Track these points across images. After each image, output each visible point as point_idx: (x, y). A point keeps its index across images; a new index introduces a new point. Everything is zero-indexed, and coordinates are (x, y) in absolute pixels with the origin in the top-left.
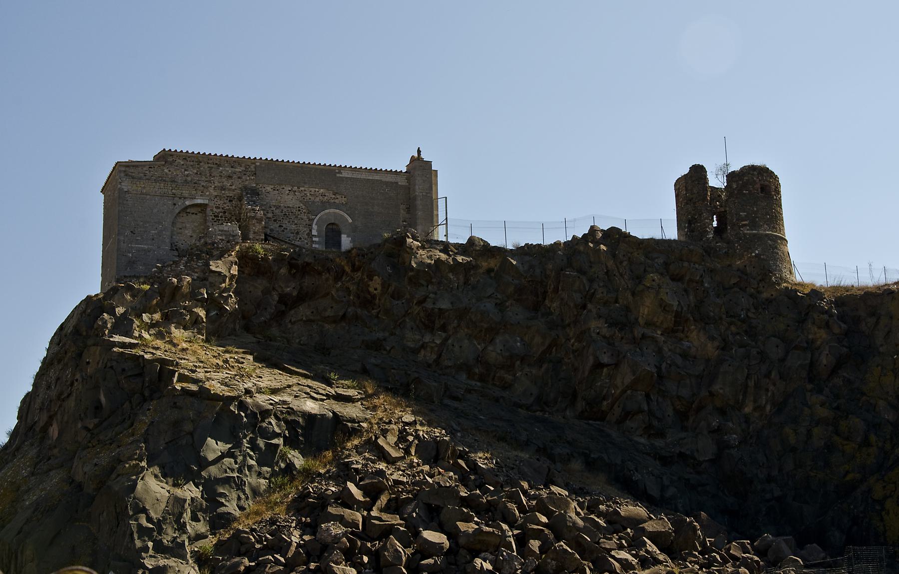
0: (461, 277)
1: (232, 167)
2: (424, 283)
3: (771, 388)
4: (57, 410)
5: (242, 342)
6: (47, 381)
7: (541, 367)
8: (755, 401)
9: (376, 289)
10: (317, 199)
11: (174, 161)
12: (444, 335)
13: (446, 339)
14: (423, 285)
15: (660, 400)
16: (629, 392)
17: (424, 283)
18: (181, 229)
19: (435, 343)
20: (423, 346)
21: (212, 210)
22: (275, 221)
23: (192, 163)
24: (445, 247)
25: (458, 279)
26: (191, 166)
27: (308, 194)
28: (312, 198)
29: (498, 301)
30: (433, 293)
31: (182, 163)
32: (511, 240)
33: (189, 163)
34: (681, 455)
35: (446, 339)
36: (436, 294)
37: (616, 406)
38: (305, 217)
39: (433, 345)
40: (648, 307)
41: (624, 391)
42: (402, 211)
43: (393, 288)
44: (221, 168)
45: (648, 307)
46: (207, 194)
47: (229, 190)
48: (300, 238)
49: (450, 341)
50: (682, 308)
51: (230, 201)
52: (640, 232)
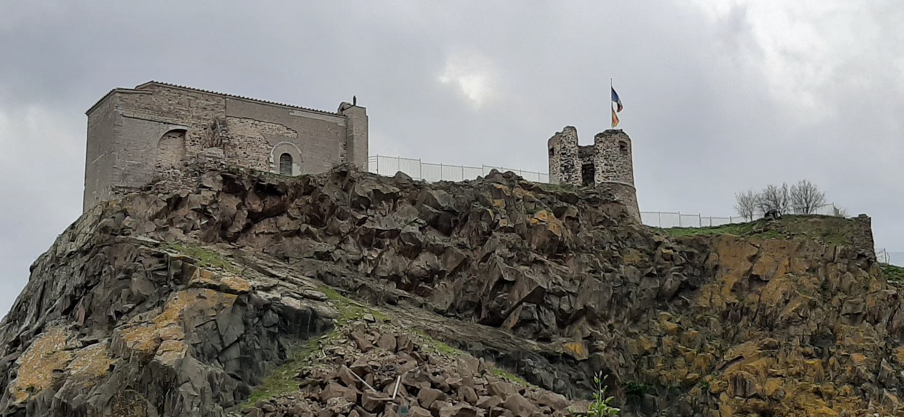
0: (392, 205)
1: (207, 100)
2: (364, 208)
3: (630, 305)
4: (539, 317)
5: (146, 246)
6: (519, 290)
7: (453, 281)
8: (616, 316)
9: (325, 211)
10: (274, 133)
11: (160, 92)
12: (379, 251)
13: (381, 254)
14: (363, 209)
15: (547, 311)
16: (524, 304)
17: (364, 208)
18: (163, 149)
19: (373, 257)
20: (363, 259)
21: (190, 136)
22: (240, 148)
23: (174, 94)
24: (379, 179)
25: (389, 206)
26: (174, 97)
27: (267, 128)
28: (270, 131)
29: (421, 226)
30: (371, 216)
31: (167, 93)
32: (431, 177)
33: (171, 94)
34: (565, 355)
35: (381, 254)
36: (373, 217)
37: (513, 314)
38: (264, 147)
39: (372, 258)
40: (539, 237)
41: (520, 303)
42: (341, 148)
43: (339, 211)
44: (198, 101)
45: (539, 237)
46: (187, 121)
47: (204, 119)
48: (260, 165)
49: (383, 256)
50: (564, 239)
51: (205, 129)
52: (529, 178)
